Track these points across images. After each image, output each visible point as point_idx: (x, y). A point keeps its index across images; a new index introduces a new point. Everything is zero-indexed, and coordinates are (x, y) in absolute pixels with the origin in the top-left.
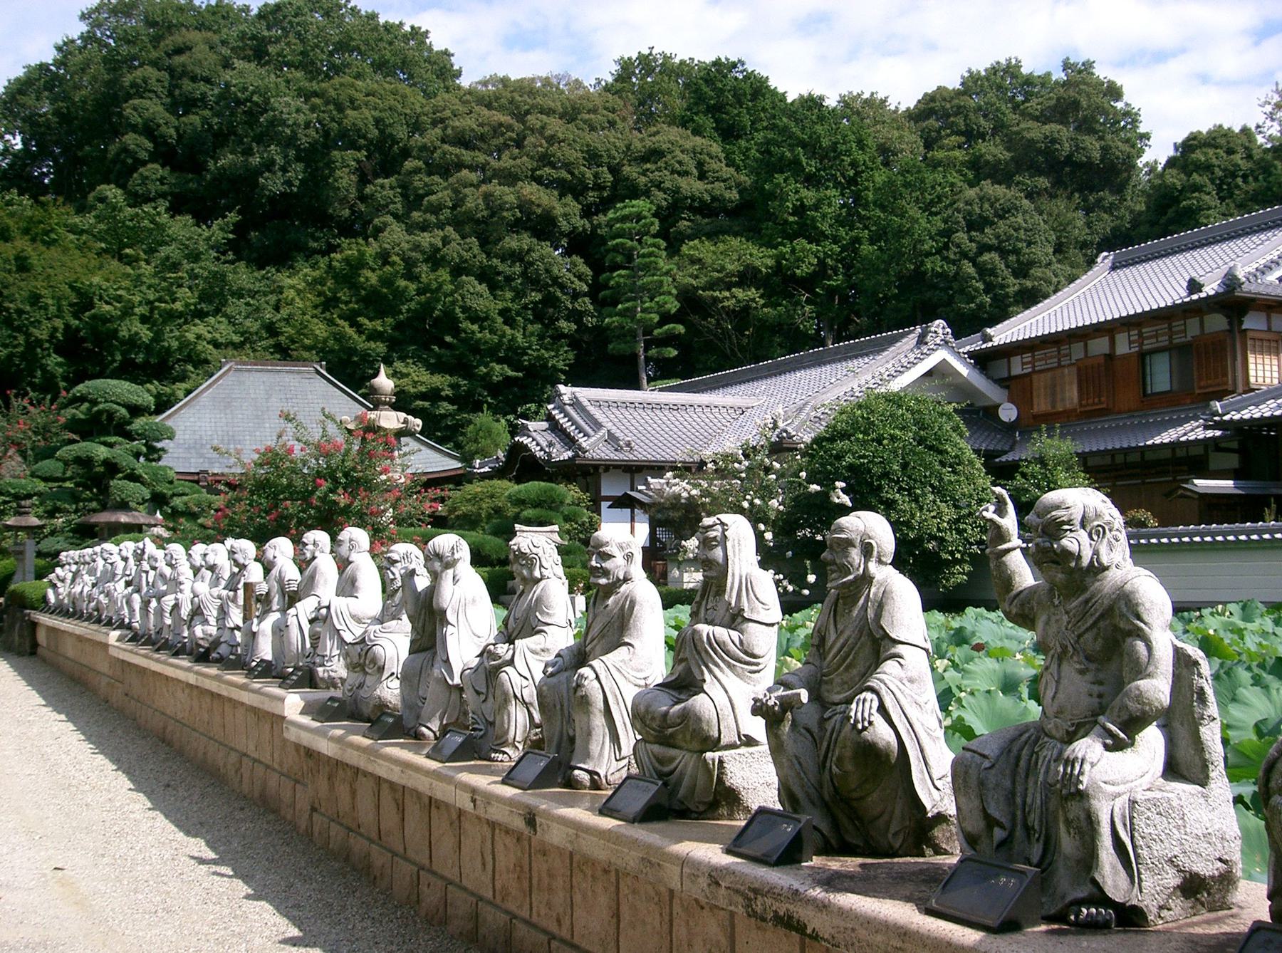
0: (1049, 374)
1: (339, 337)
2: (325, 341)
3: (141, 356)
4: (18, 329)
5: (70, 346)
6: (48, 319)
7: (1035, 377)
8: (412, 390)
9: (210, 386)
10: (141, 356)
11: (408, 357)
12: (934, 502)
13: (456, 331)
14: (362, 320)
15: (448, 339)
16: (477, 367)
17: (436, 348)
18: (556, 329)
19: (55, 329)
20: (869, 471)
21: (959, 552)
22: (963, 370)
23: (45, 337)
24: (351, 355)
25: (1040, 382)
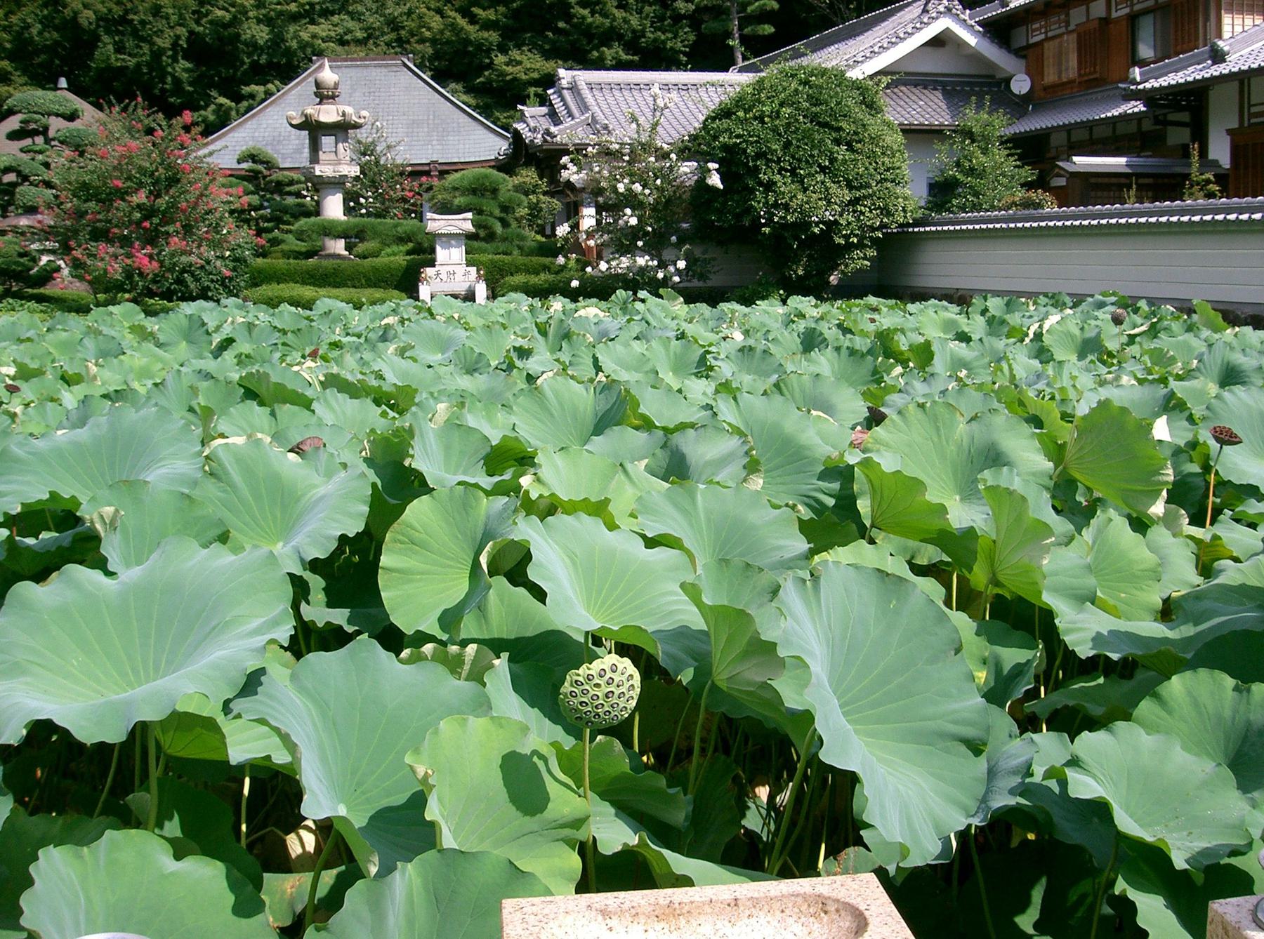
0: (1057, 41)
1: (453, 26)
2: (442, 32)
3: (264, 57)
4: (143, 39)
5: (196, 50)
6: (172, 28)
7: (1046, 45)
8: (524, 77)
9: (298, 84)
10: (264, 57)
11: (524, 44)
12: (823, 182)
13: (568, 17)
14: (475, 10)
15: (561, 25)
16: (590, 51)
17: (550, 34)
18: (674, 10)
19: (178, 37)
20: (745, 151)
21: (856, 236)
22: (971, 40)
23: (167, 45)
24: (466, 46)
25: (1050, 49)
